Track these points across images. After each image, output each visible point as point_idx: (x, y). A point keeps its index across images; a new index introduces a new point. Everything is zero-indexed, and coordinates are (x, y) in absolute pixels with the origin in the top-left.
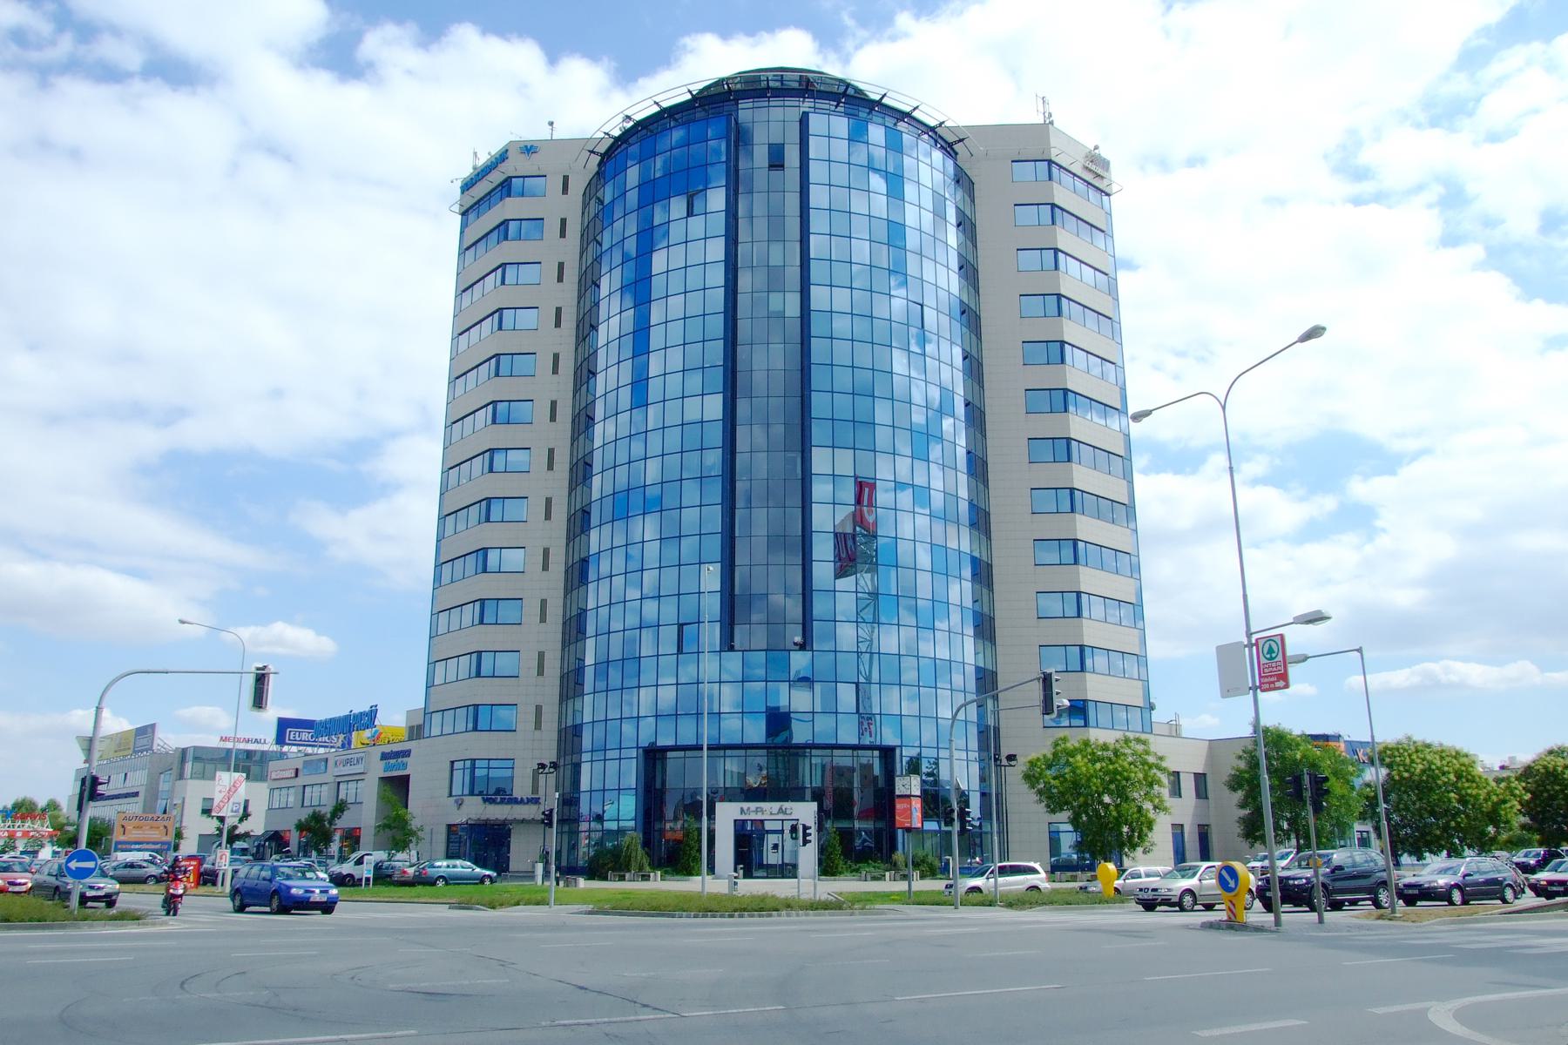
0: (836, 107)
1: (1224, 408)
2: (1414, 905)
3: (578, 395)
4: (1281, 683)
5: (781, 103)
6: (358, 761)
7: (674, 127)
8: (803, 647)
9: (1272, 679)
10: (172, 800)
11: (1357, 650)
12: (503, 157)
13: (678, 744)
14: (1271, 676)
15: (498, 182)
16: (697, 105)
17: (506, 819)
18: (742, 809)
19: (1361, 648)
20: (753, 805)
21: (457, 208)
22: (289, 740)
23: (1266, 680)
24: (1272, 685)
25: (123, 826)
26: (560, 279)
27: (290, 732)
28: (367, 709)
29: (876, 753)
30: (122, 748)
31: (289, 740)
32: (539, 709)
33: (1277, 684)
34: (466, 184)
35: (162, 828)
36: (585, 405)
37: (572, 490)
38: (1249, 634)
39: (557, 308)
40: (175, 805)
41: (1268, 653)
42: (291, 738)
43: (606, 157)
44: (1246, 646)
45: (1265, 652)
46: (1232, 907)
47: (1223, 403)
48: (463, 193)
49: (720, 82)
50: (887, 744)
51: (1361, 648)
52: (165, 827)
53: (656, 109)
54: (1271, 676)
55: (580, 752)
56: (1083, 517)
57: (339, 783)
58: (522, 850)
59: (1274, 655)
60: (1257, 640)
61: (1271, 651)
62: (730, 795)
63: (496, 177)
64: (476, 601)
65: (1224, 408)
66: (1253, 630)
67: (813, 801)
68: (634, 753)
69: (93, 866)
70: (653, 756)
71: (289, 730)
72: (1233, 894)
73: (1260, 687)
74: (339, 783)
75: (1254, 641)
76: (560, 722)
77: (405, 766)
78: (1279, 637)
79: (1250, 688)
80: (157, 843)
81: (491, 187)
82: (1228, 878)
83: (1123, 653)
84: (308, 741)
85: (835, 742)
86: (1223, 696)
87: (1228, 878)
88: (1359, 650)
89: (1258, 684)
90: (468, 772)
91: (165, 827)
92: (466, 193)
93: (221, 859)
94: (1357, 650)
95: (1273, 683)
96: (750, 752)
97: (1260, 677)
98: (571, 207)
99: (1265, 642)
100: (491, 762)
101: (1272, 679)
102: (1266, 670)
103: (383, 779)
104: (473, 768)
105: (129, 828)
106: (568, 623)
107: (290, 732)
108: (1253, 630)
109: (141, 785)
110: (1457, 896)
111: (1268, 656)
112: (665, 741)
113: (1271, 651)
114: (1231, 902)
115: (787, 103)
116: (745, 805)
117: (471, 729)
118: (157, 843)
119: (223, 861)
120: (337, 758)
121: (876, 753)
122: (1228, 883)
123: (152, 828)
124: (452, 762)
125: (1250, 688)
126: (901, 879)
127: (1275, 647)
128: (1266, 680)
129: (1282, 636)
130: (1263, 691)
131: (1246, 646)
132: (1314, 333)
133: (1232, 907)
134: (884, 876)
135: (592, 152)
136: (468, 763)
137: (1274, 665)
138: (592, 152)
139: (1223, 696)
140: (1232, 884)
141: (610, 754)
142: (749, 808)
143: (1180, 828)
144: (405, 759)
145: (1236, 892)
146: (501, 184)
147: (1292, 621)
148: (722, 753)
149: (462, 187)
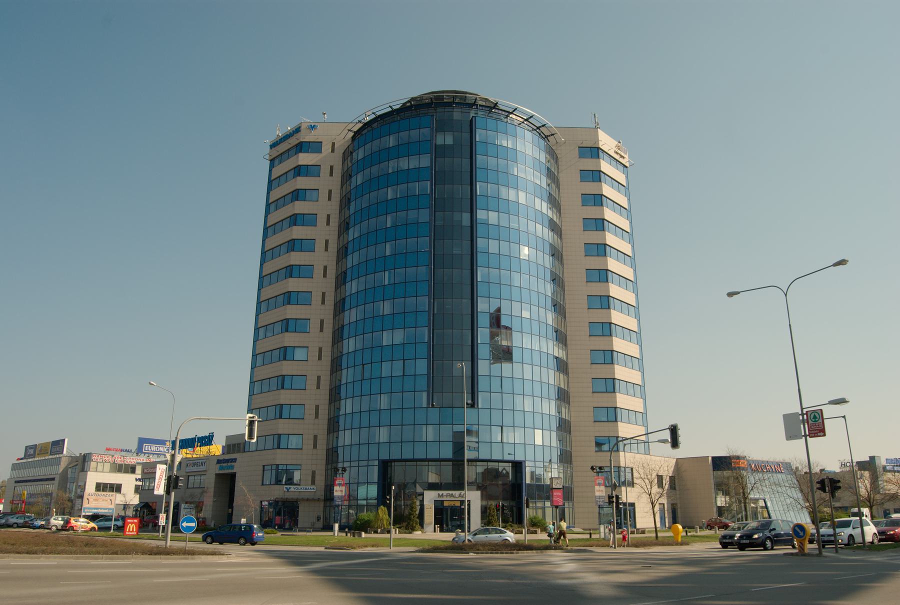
0: (489, 114)
1: (786, 295)
2: (726, 548)
3: (340, 263)
4: (822, 434)
5: (443, 110)
6: (202, 464)
7: (392, 122)
8: (473, 405)
9: (816, 432)
10: (77, 483)
11: (843, 417)
12: (297, 130)
13: (403, 458)
14: (815, 430)
15: (294, 144)
16: (413, 109)
17: (297, 499)
18: (439, 494)
19: (845, 416)
20: (445, 493)
21: (267, 157)
22: (145, 450)
23: (813, 432)
24: (816, 435)
25: (88, 499)
26: (330, 199)
27: (145, 446)
28: (207, 435)
29: (510, 464)
30: (43, 452)
31: (145, 450)
32: (315, 437)
33: (819, 434)
34: (274, 144)
35: (109, 501)
36: (342, 245)
37: (335, 316)
38: (802, 409)
39: (328, 215)
40: (80, 486)
41: (813, 418)
42: (146, 449)
43: (357, 133)
44: (800, 415)
45: (812, 418)
46: (801, 545)
47: (785, 293)
48: (271, 148)
49: (413, 99)
50: (405, 458)
51: (845, 416)
52: (111, 500)
53: (390, 109)
54: (815, 430)
55: (337, 462)
56: (616, 338)
57: (189, 476)
58: (305, 514)
59: (817, 420)
60: (807, 412)
61: (815, 417)
62: (433, 487)
63: (293, 141)
64: (280, 376)
65: (786, 295)
66: (804, 407)
67: (477, 490)
68: (376, 463)
69: (194, 526)
70: (385, 466)
71: (145, 445)
72: (802, 539)
73: (809, 435)
74: (189, 476)
75: (805, 412)
76: (328, 444)
77: (233, 467)
78: (820, 411)
79: (803, 436)
80: (106, 509)
81: (290, 146)
82: (798, 530)
83: (636, 411)
84: (156, 451)
85: (502, 459)
86: (787, 439)
87: (798, 530)
88: (844, 417)
89: (807, 434)
90: (274, 472)
91: (111, 500)
92: (273, 149)
93: (162, 519)
94: (843, 417)
95: (817, 433)
96: (407, 463)
97: (809, 430)
98: (336, 160)
99: (811, 413)
100: (287, 466)
101: (816, 432)
102: (812, 427)
103: (217, 475)
104: (277, 469)
105: (90, 500)
106: (335, 360)
107: (145, 446)
108: (804, 407)
109: (56, 474)
110: (769, 544)
111: (814, 420)
112: (396, 455)
113: (815, 417)
114: (800, 542)
115: (446, 110)
116: (441, 492)
117: (276, 447)
118: (106, 509)
119: (163, 520)
120: (188, 462)
121: (510, 464)
122: (799, 533)
123: (103, 500)
124: (264, 466)
125: (803, 436)
126: (387, 533)
127: (818, 416)
128: (813, 432)
129: (821, 410)
130: (810, 437)
131: (800, 415)
132: (842, 262)
133: (801, 545)
134: (599, 529)
135: (349, 130)
136: (274, 467)
137: (817, 424)
138: (349, 130)
139: (787, 439)
140: (801, 534)
141: (356, 464)
142: (443, 494)
143: (662, 505)
144: (233, 464)
145: (804, 537)
146: (296, 145)
147: (828, 403)
148: (426, 463)
149: (270, 146)
